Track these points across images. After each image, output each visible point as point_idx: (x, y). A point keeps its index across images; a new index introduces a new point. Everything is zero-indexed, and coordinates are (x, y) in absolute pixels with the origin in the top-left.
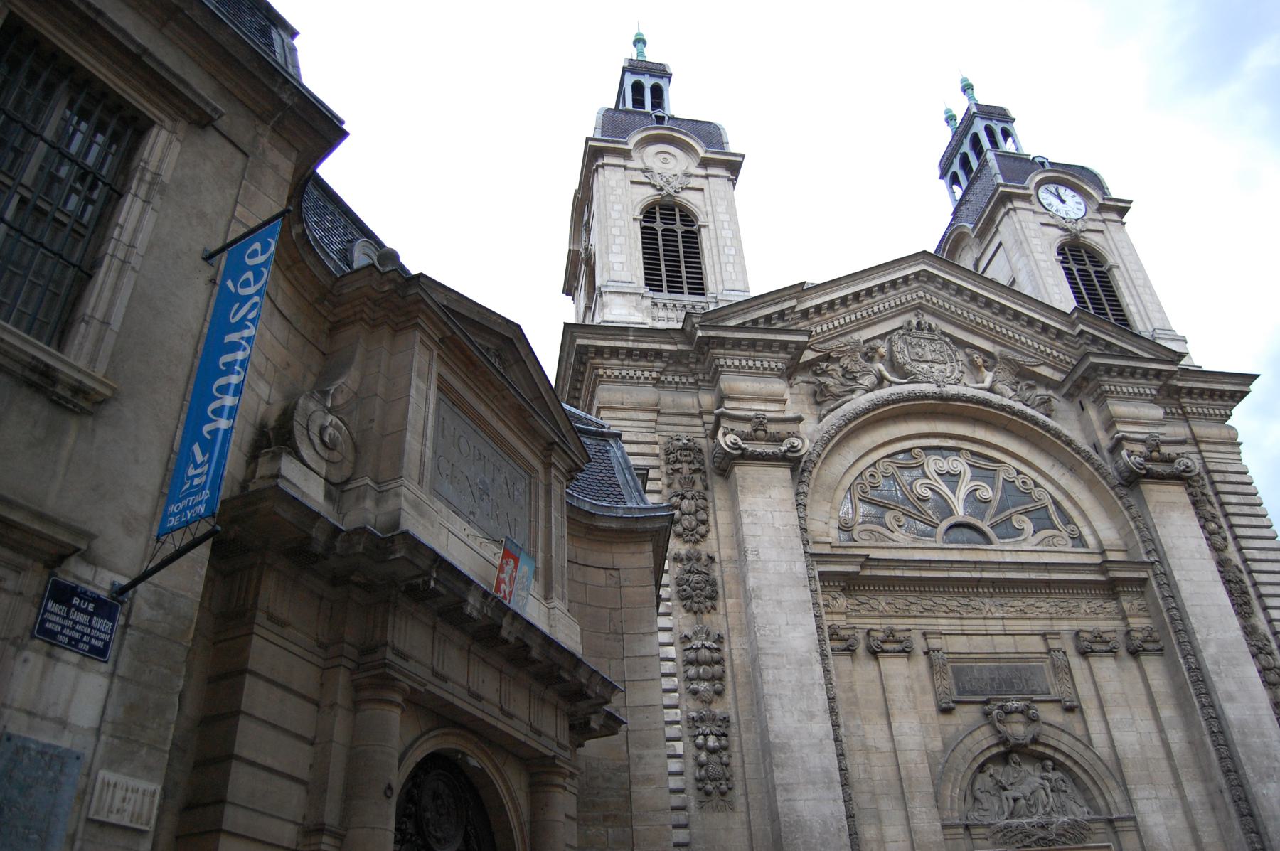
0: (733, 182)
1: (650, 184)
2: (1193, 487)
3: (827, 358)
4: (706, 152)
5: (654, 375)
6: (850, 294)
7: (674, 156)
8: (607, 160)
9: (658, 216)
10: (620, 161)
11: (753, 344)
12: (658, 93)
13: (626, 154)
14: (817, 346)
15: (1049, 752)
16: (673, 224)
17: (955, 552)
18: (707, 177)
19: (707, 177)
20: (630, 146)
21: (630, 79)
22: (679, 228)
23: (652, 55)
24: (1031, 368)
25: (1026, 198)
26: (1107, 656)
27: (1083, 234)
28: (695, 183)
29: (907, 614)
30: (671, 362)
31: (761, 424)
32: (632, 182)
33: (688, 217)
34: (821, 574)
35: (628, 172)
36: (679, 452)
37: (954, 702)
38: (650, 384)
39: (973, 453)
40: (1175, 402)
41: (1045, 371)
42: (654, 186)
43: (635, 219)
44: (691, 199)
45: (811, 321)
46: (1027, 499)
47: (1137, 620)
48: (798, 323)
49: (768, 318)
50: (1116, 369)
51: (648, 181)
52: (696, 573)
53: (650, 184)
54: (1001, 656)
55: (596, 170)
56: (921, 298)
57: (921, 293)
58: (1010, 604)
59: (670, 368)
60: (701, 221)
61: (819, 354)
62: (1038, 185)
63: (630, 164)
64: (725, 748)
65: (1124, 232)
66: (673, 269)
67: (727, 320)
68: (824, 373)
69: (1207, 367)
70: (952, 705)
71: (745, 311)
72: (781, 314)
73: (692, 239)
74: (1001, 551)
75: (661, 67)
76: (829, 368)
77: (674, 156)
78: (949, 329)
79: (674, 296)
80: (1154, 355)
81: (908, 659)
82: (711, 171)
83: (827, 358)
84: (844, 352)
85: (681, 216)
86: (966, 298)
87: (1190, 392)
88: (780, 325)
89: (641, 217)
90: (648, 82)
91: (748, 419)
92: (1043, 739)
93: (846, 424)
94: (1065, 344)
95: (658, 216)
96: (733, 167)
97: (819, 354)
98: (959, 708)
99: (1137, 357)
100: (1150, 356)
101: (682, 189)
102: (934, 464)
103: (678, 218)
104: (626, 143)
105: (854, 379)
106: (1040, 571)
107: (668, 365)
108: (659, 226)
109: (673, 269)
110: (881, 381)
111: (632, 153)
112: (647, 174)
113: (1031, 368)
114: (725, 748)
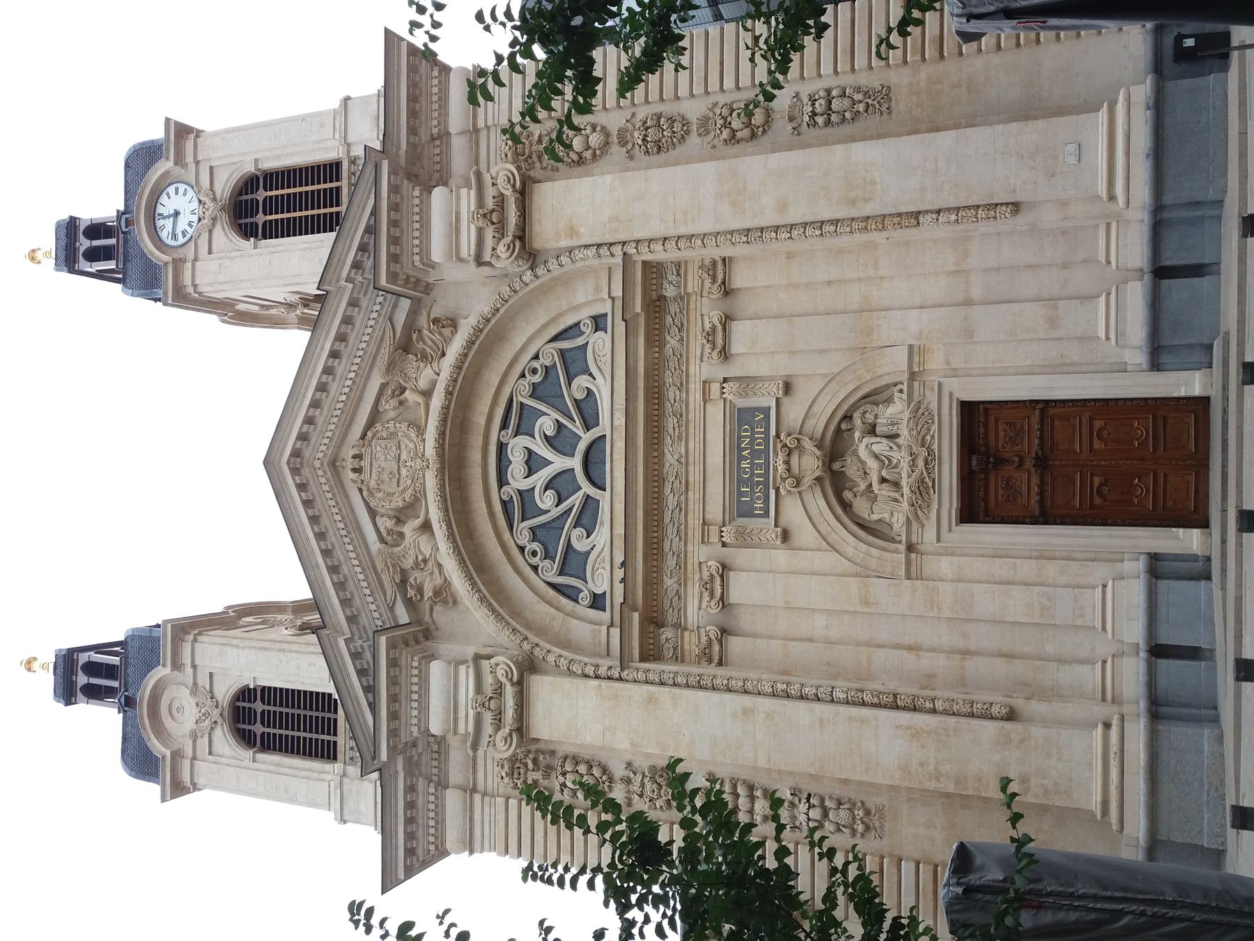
0: (198, 133)
1: (210, 231)
2: (531, 153)
3: (403, 584)
4: (167, 159)
5: (432, 790)
6: (325, 562)
7: (170, 706)
8: (187, 280)
9: (249, 220)
10: (186, 764)
11: (393, 698)
12: (96, 230)
13: (177, 755)
14: (388, 598)
15: (832, 428)
16: (255, 712)
17: (615, 473)
18: (197, 163)
19: (197, 163)
20: (168, 753)
21: (85, 265)
22: (261, 195)
23: (48, 242)
24: (398, 335)
25: (178, 264)
26: (727, 580)
27: (218, 196)
28: (203, 681)
29: (682, 556)
30: (417, 772)
31: (485, 216)
32: (210, 253)
33: (250, 183)
34: (643, 659)
35: (200, 257)
36: (516, 781)
37: (776, 526)
38: (445, 77)
39: (504, 425)
40: (426, 148)
41: (400, 318)
42: (212, 729)
43: (255, 247)
44: (225, 184)
45: (361, 609)
46: (552, 373)
47: (690, 285)
48: (364, 626)
49: (361, 673)
50: (392, 247)
51: (207, 735)
52: (643, 787)
53: (210, 734)
54: (727, 504)
55: (200, 293)
56: (322, 464)
57: (317, 464)
58: (671, 431)
59: (424, 771)
60: (250, 168)
61: (398, 598)
62: (160, 244)
63: (189, 752)
64: (822, 800)
65: (215, 134)
66: (311, 200)
67: (366, 725)
68: (420, 590)
69: (380, 82)
70: (779, 529)
71: (355, 703)
72: (355, 656)
73: (274, 178)
74: (611, 420)
75: (61, 661)
76: (413, 583)
77: (170, 706)
78: (357, 430)
79: (345, 174)
80: (370, 192)
81: (730, 570)
82: (187, 660)
83: (403, 584)
84: (393, 565)
85: (246, 194)
86: (317, 414)
87: (412, 131)
88: (368, 655)
89: (252, 239)
90: (84, 244)
91: (480, 232)
92: (818, 434)
93: (479, 591)
94: (365, 295)
95: (249, 220)
96: (181, 132)
97: (398, 598)
98: (783, 521)
99: (375, 212)
100: (373, 196)
101: (212, 698)
102: (518, 480)
103: (249, 197)
104: (164, 757)
105: (425, 561)
106: (635, 425)
107: (421, 775)
108: (261, 218)
109: (311, 200)
110: (426, 527)
111: (176, 748)
112: (199, 735)
113: (398, 335)
114: (822, 800)
